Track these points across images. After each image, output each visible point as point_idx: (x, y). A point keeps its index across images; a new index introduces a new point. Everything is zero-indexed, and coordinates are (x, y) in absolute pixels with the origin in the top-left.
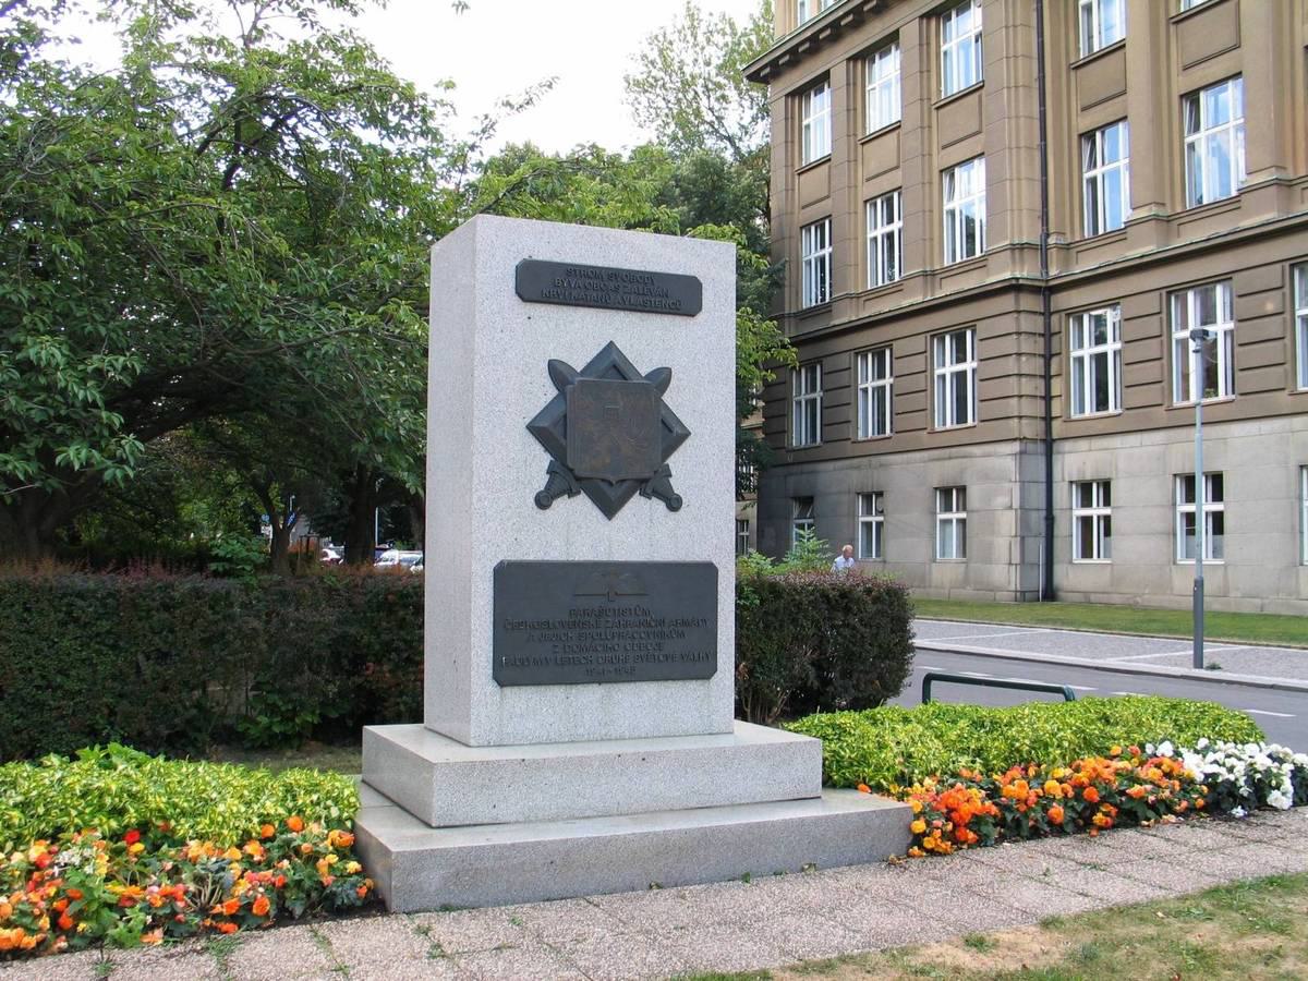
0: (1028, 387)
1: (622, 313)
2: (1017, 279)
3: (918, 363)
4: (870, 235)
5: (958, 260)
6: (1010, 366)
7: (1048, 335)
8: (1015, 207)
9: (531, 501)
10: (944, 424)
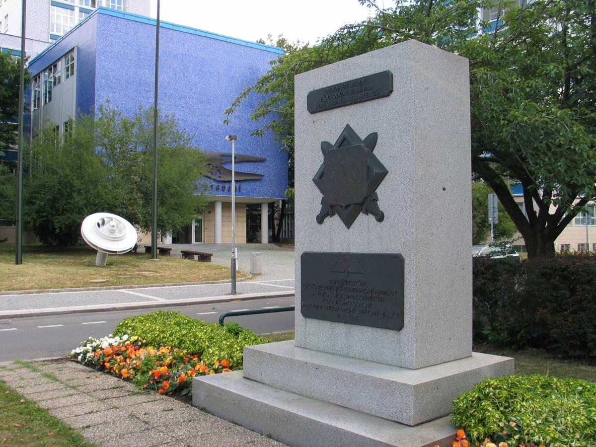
1: (353, 106)
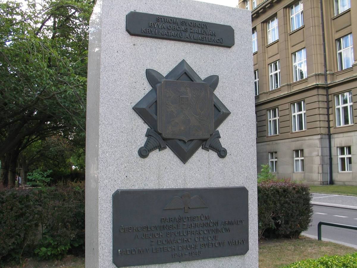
0: (322, 118)
2: (318, 84)
3: (287, 112)
4: (270, 74)
5: (298, 80)
6: (316, 111)
7: (328, 102)
8: (316, 63)
9: (136, 153)
10: (296, 130)
